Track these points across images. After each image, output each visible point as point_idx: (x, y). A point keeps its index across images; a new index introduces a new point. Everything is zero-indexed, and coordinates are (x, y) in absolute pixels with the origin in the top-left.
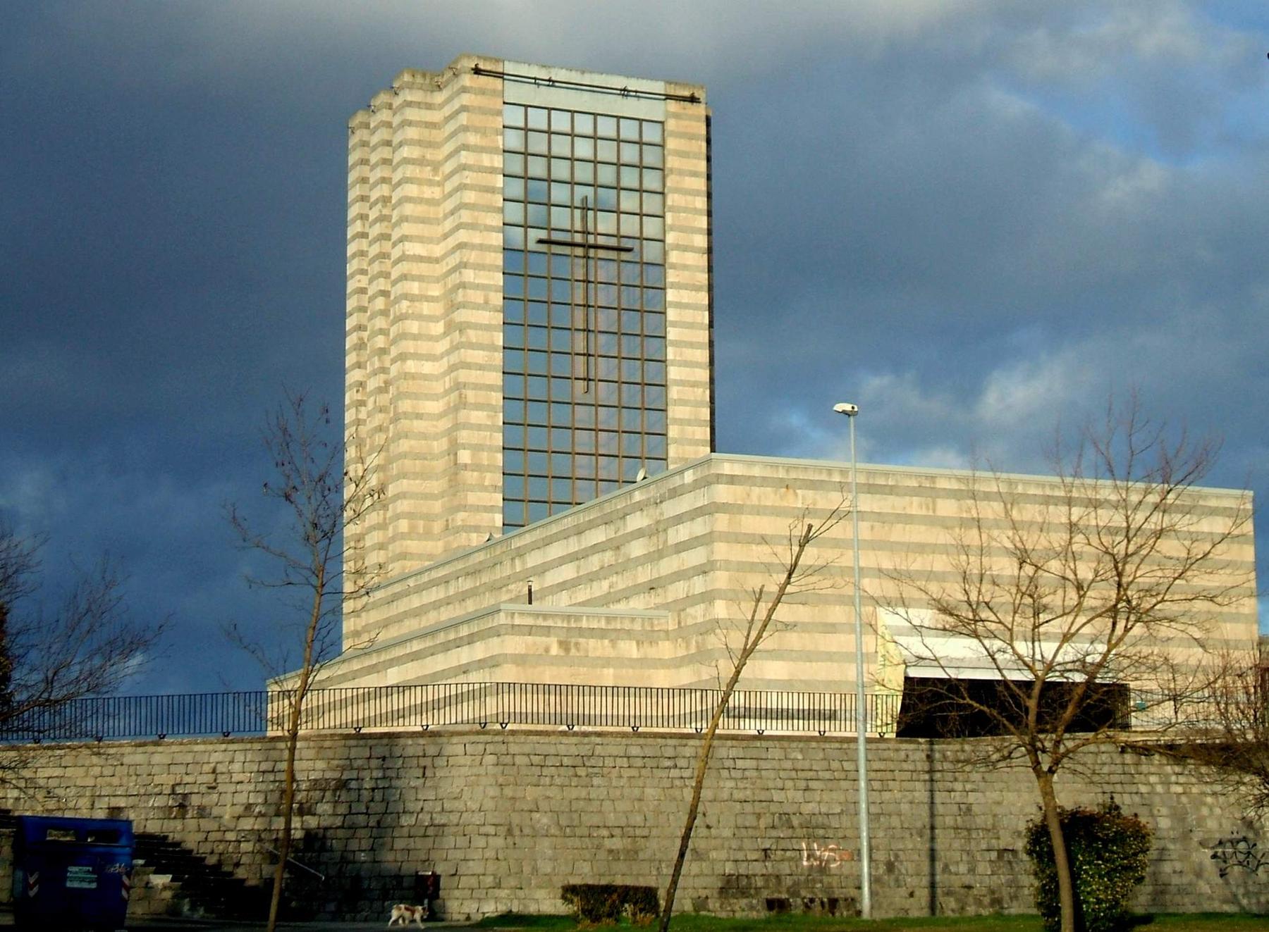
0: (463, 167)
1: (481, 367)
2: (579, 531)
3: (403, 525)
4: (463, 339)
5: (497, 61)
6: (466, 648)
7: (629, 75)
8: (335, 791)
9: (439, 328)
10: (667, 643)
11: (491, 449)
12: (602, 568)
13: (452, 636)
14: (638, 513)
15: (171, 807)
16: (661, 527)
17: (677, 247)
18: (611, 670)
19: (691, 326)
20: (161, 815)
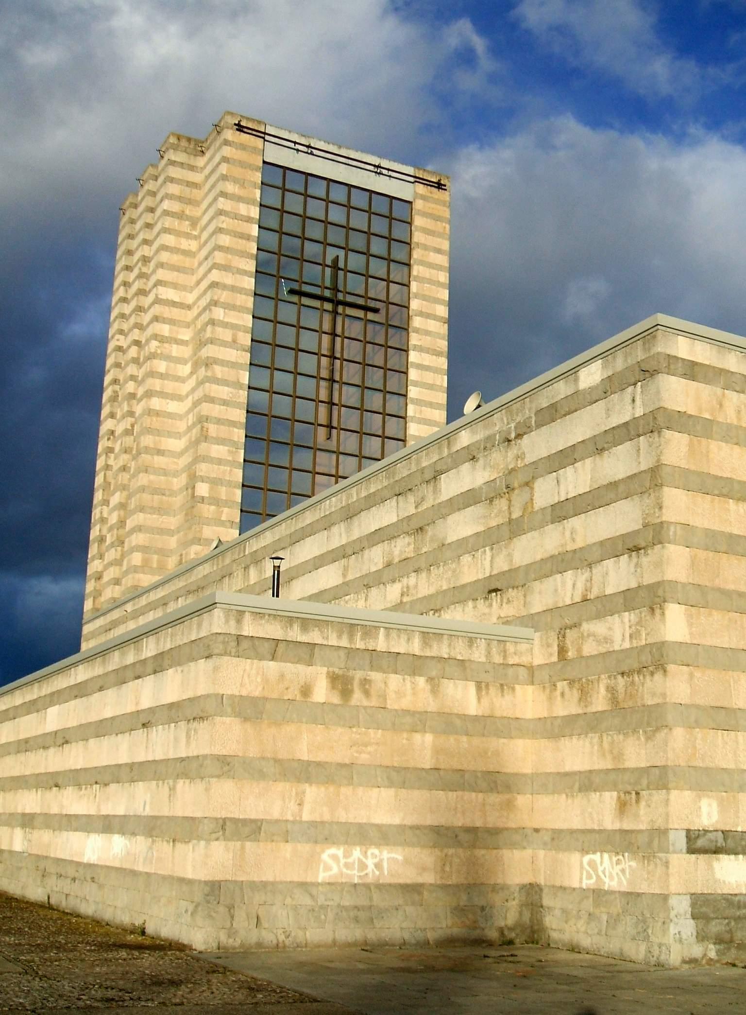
1: (225, 403)
2: (349, 515)
4: (209, 374)
6: (149, 680)
7: (380, 156)
9: (187, 369)
10: (530, 689)
11: (230, 484)
12: (389, 565)
13: (131, 658)
14: (466, 466)
16: (521, 478)
17: (421, 314)
18: (429, 738)
19: (431, 387)
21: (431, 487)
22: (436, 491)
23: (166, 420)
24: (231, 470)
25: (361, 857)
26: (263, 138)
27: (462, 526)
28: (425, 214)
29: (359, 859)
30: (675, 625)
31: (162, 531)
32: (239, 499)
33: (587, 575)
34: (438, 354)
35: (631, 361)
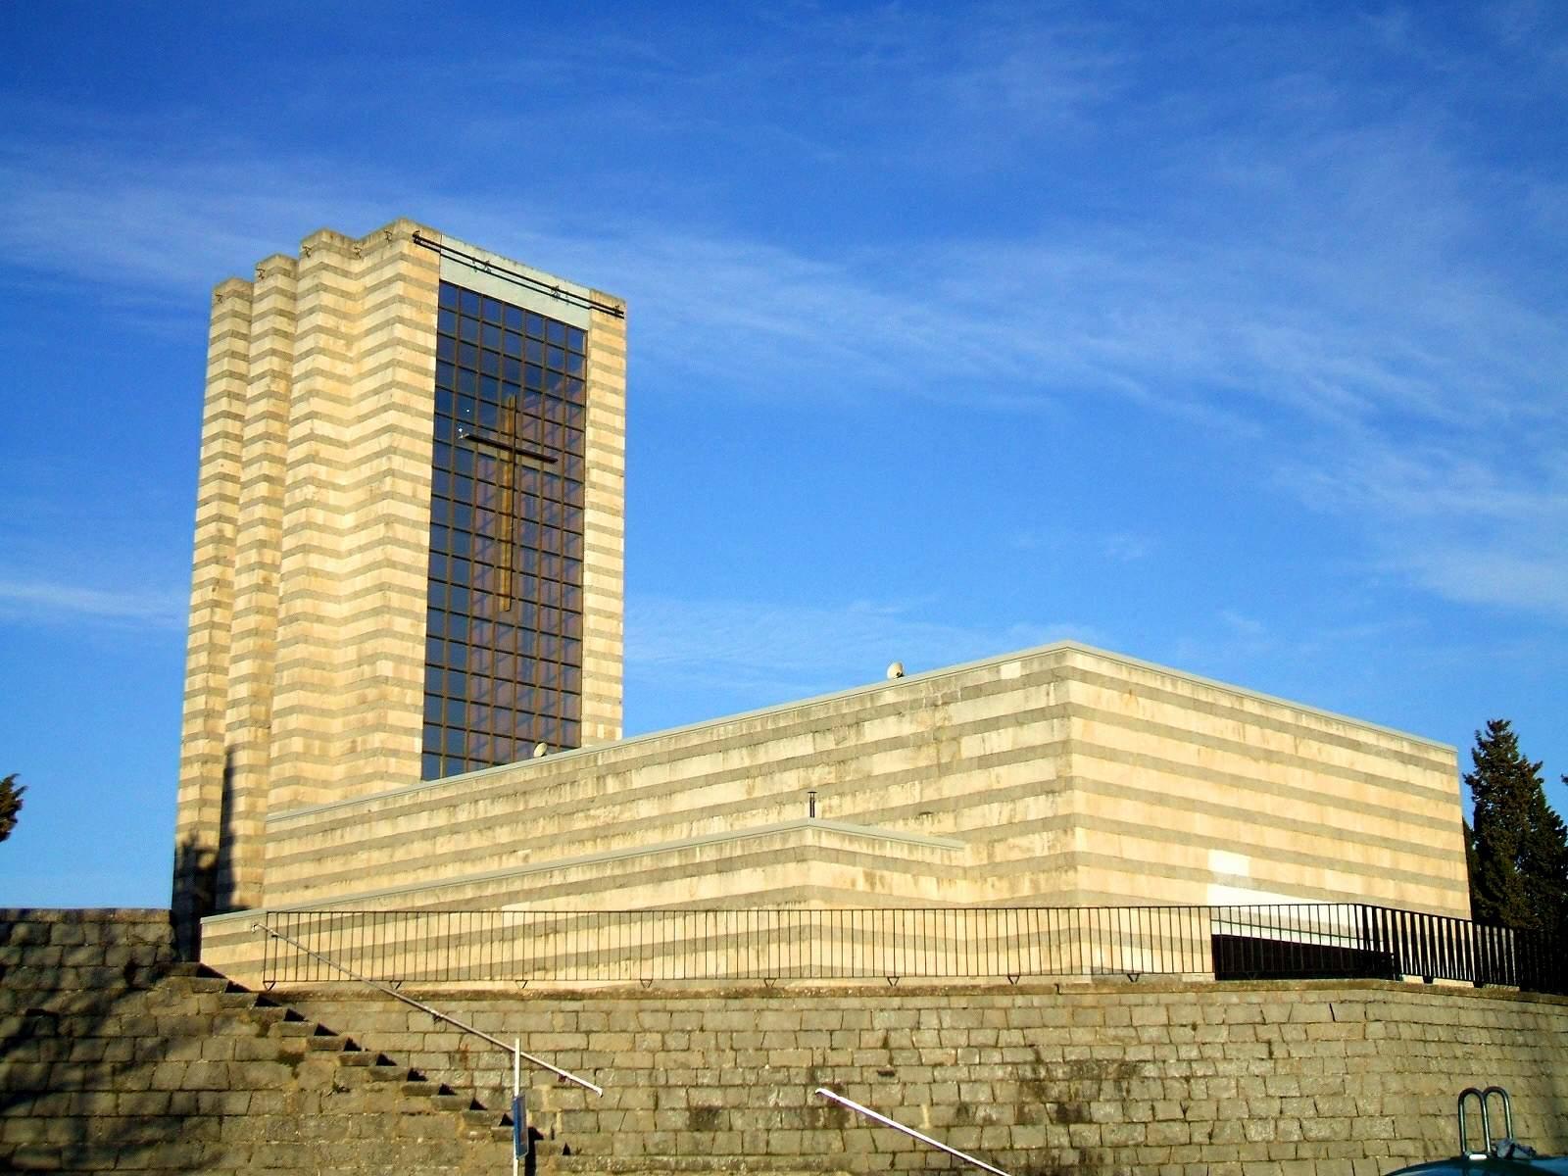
0: (399, 342)
3: (297, 744)
4: (390, 534)
5: (436, 232)
8: (1117, 1081)
15: (814, 1109)
19: (608, 551)
20: (797, 1123)
21: (853, 731)
22: (859, 733)
23: (325, 581)
24: (414, 647)
27: (885, 764)
28: (601, 347)
30: (1080, 841)
31: (324, 713)
32: (422, 680)
33: (1011, 806)
34: (615, 513)
35: (1045, 667)
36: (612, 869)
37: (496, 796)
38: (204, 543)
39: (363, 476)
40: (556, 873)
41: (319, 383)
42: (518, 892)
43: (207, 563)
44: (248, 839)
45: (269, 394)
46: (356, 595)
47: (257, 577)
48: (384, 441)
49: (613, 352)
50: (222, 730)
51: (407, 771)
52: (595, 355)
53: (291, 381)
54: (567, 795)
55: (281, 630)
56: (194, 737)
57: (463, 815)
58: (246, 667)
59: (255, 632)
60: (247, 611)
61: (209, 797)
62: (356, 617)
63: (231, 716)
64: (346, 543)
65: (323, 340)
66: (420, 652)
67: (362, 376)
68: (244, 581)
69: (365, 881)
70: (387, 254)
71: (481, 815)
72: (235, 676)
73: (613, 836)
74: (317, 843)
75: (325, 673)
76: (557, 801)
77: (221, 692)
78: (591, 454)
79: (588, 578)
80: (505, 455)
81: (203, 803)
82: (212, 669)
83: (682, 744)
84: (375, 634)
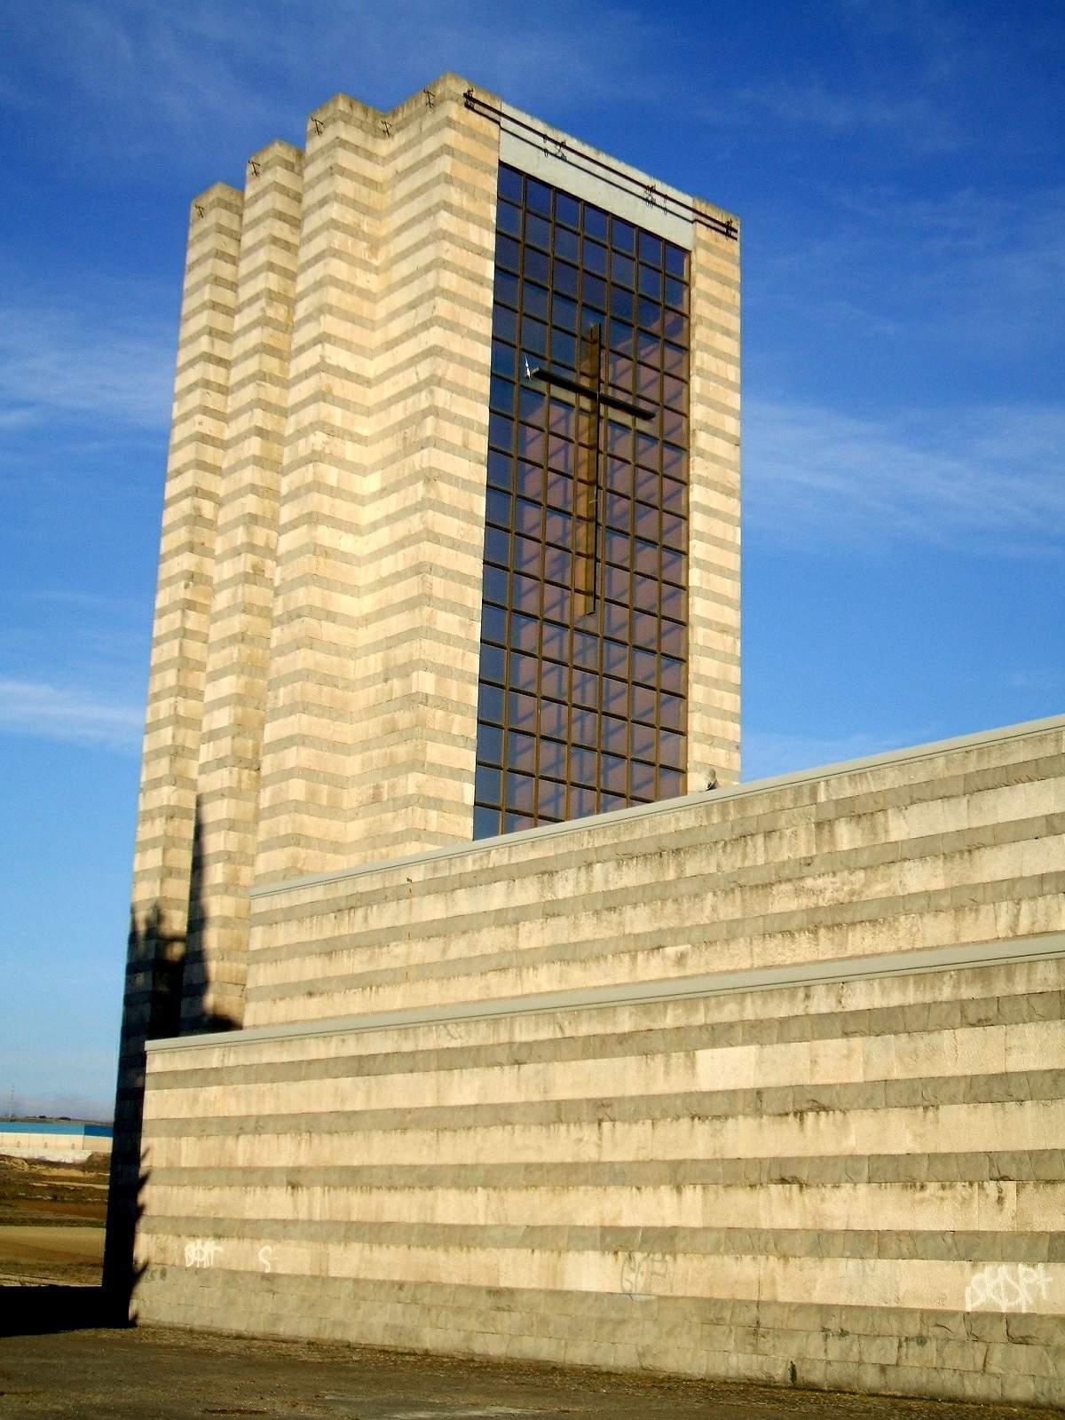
0: (444, 235)
3: (297, 789)
4: (432, 495)
17: (707, 428)
19: (720, 543)
23: (338, 564)
24: (464, 654)
25: (1009, 1279)
26: (498, 123)
28: (709, 274)
29: (1005, 1281)
34: (728, 492)
36: (957, 986)
37: (625, 856)
38: (174, 526)
39: (392, 421)
40: (819, 991)
41: (333, 295)
42: (731, 1026)
43: (178, 551)
44: (226, 922)
45: (264, 322)
46: (382, 583)
47: (245, 563)
48: (424, 370)
49: (725, 281)
50: (194, 774)
51: (456, 831)
52: (701, 283)
53: (291, 303)
54: (758, 854)
55: (276, 632)
56: (156, 783)
57: (565, 887)
58: (228, 685)
59: (241, 638)
60: (231, 610)
61: (175, 864)
62: (381, 614)
63: (207, 753)
64: (367, 515)
65: (338, 240)
66: (473, 663)
67: (391, 289)
68: (227, 570)
69: (402, 987)
70: (428, 123)
71: (599, 887)
72: (214, 698)
73: (853, 924)
74: (327, 928)
75: (338, 692)
76: (739, 864)
77: (192, 723)
78: (698, 412)
79: (695, 578)
80: (586, 403)
81: (167, 872)
82: (183, 691)
83: (994, 762)
84: (411, 635)
